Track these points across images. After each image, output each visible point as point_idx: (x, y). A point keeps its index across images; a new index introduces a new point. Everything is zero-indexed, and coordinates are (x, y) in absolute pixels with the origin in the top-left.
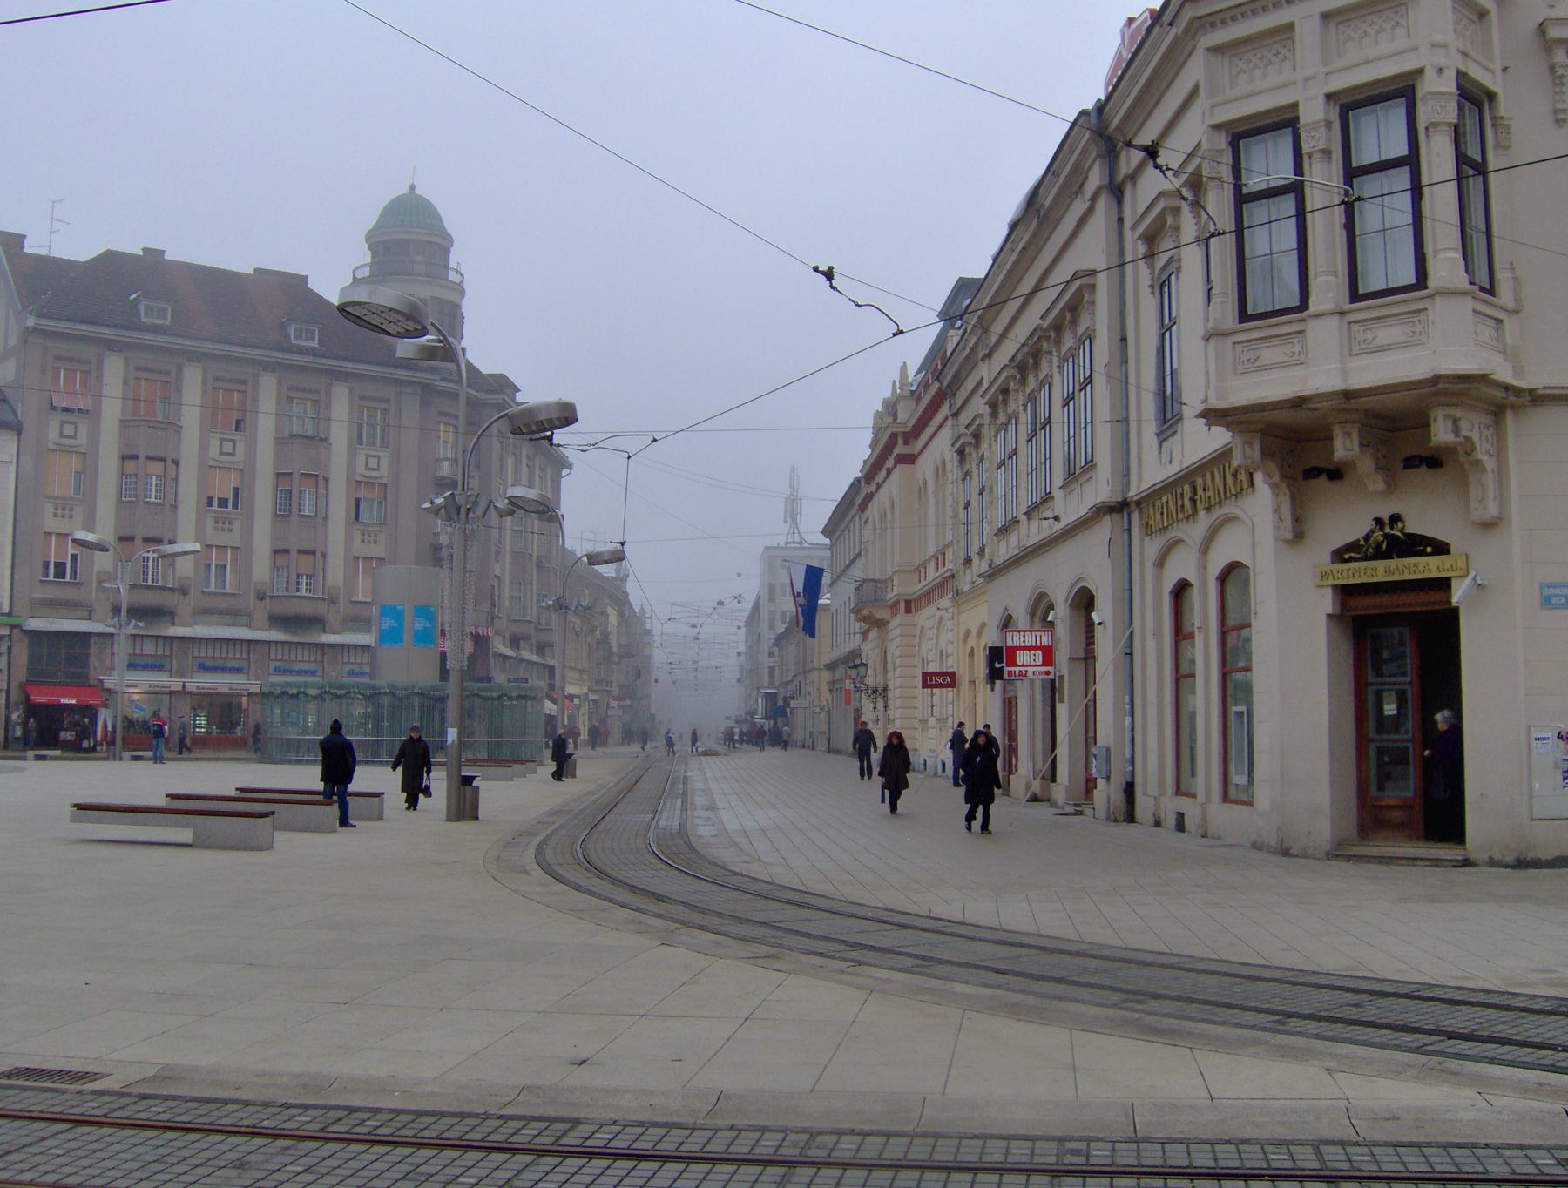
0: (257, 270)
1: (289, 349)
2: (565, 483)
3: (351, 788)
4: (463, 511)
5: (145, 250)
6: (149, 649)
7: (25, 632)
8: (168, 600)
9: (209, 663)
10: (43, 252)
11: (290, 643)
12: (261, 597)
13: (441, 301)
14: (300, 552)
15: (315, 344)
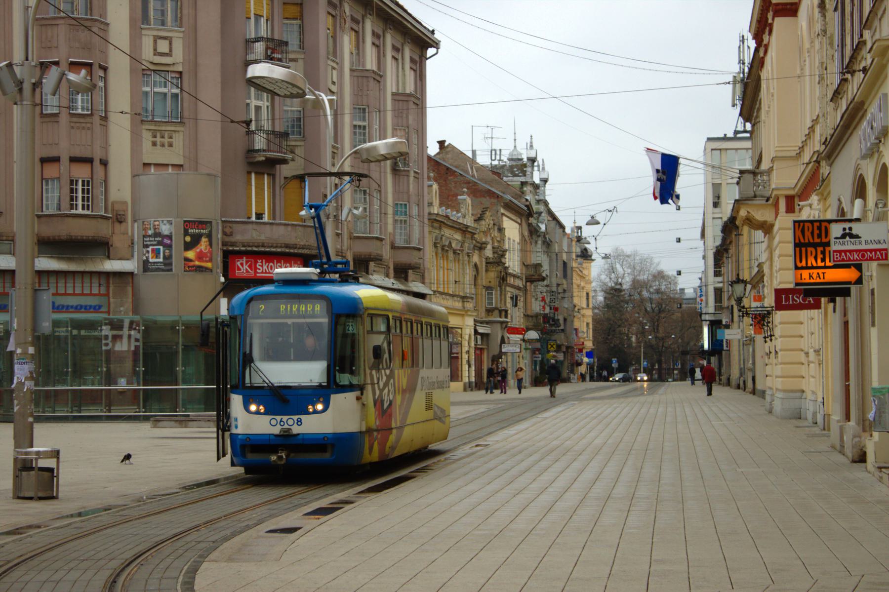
2: (431, 66)
4: (27, 87)
8: (102, 230)
11: (74, 273)
14: (74, 160)
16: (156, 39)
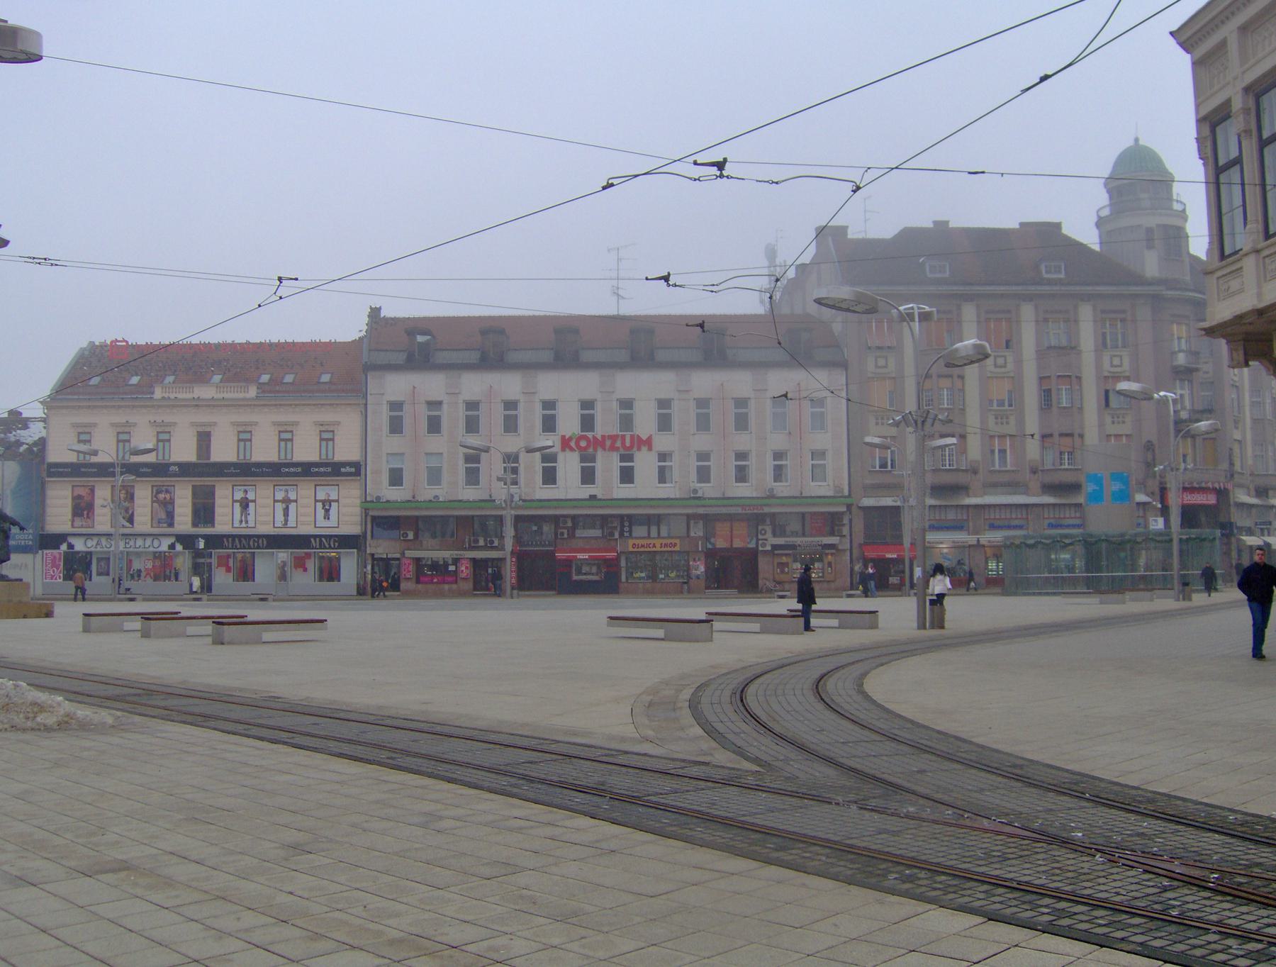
0: (1021, 224)
1: (1042, 282)
3: (814, 607)
5: (935, 222)
6: (951, 515)
7: (860, 508)
8: (962, 479)
9: (997, 523)
10: (860, 236)
11: (1060, 505)
12: (1034, 471)
13: (1166, 227)
14: (1061, 435)
15: (1062, 276)
16: (1112, 357)
